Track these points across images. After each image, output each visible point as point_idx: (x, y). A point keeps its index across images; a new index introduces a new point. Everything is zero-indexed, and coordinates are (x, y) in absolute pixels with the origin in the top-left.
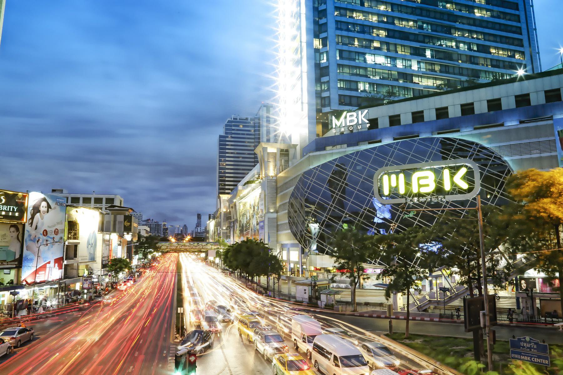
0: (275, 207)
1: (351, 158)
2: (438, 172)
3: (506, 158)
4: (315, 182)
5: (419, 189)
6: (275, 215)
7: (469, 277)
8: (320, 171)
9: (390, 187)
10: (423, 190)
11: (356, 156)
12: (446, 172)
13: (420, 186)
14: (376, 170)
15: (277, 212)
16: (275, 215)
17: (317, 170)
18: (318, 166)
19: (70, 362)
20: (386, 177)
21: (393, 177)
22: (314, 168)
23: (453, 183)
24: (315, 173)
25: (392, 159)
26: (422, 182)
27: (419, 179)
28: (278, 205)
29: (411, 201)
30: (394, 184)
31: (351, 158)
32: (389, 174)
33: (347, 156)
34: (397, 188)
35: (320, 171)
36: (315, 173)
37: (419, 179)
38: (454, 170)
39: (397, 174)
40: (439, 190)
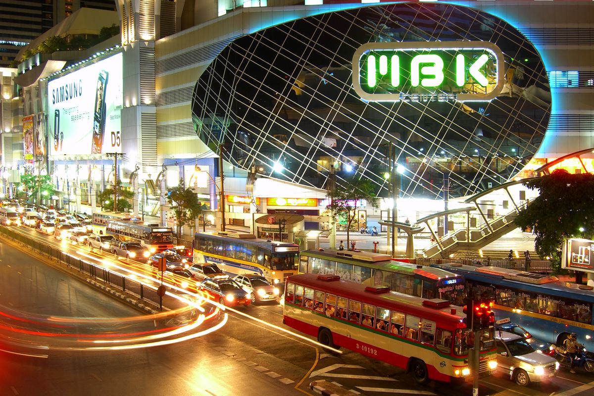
0: (153, 95)
1: (317, 23)
2: (449, 59)
3: (537, 47)
4: (297, 60)
5: (420, 81)
6: (153, 110)
7: (34, 203)
8: (263, 40)
9: (379, 76)
10: (426, 83)
11: (324, 21)
12: (460, 60)
13: (422, 77)
14: (358, 46)
15: (156, 104)
16: (153, 110)
17: (258, 37)
18: (261, 32)
19: (57, 348)
20: (371, 60)
21: (383, 59)
22: (254, 35)
23: (468, 76)
24: (256, 42)
25: (318, 27)
26: (426, 71)
27: (422, 66)
28: (158, 91)
29: (407, 98)
30: (383, 71)
31: (317, 23)
32: (377, 55)
33: (310, 19)
34: (387, 77)
35: (263, 40)
36: (256, 42)
37: (422, 66)
38: (471, 58)
39: (389, 55)
40: (449, 85)
